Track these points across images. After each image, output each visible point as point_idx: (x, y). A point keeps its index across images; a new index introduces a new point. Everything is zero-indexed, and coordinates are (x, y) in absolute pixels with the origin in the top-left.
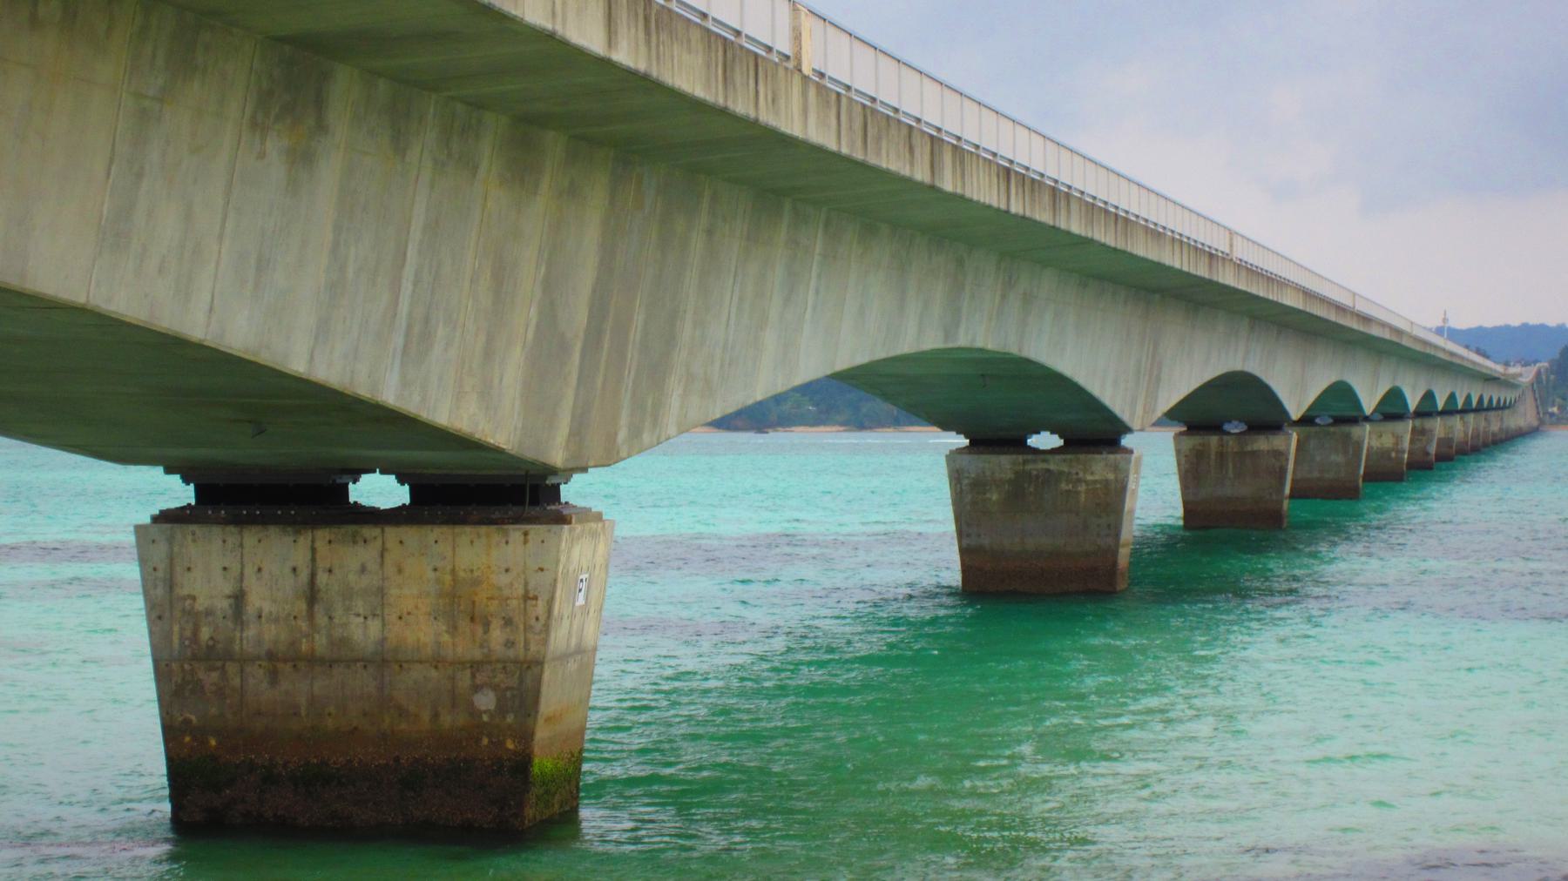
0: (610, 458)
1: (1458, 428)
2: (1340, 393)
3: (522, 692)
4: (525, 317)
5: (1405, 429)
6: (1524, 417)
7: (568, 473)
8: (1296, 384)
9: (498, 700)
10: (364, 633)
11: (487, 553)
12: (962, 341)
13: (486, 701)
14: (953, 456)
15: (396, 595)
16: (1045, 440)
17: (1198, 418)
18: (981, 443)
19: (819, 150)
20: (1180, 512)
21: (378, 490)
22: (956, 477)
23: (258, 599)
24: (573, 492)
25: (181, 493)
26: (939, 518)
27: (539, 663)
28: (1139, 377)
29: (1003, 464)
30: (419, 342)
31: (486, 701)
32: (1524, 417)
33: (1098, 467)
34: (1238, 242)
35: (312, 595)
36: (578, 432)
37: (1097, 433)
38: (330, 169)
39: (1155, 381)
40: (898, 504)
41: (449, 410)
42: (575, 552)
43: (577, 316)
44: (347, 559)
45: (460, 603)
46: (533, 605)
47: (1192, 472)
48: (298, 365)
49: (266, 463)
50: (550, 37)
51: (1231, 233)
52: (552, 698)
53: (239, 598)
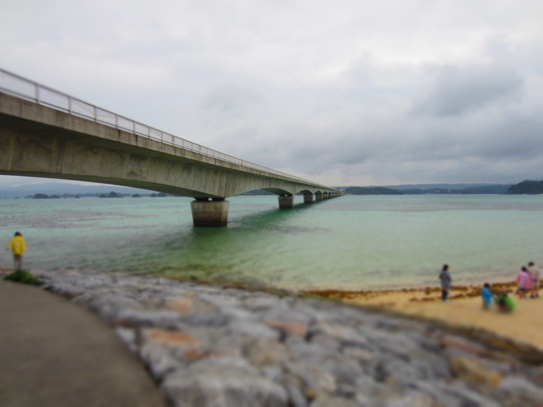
0: (229, 196)
1: (334, 195)
3: (220, 214)
5: (327, 195)
7: (225, 197)
8: (322, 191)
9: (305, 198)
10: (208, 210)
11: (218, 204)
12: (271, 187)
15: (210, 207)
16: (286, 196)
19: (245, 172)
21: (210, 199)
24: (226, 199)
25: (194, 199)
28: (313, 191)
29: (282, 197)
30: (205, 187)
32: (343, 193)
33: (290, 198)
34: (176, 139)
37: (311, 194)
38: (192, 174)
39: (295, 191)
42: (224, 204)
43: (224, 185)
44: (207, 205)
45: (216, 208)
46: (221, 208)
47: (316, 197)
49: (201, 198)
50: (207, 163)
51: (173, 136)
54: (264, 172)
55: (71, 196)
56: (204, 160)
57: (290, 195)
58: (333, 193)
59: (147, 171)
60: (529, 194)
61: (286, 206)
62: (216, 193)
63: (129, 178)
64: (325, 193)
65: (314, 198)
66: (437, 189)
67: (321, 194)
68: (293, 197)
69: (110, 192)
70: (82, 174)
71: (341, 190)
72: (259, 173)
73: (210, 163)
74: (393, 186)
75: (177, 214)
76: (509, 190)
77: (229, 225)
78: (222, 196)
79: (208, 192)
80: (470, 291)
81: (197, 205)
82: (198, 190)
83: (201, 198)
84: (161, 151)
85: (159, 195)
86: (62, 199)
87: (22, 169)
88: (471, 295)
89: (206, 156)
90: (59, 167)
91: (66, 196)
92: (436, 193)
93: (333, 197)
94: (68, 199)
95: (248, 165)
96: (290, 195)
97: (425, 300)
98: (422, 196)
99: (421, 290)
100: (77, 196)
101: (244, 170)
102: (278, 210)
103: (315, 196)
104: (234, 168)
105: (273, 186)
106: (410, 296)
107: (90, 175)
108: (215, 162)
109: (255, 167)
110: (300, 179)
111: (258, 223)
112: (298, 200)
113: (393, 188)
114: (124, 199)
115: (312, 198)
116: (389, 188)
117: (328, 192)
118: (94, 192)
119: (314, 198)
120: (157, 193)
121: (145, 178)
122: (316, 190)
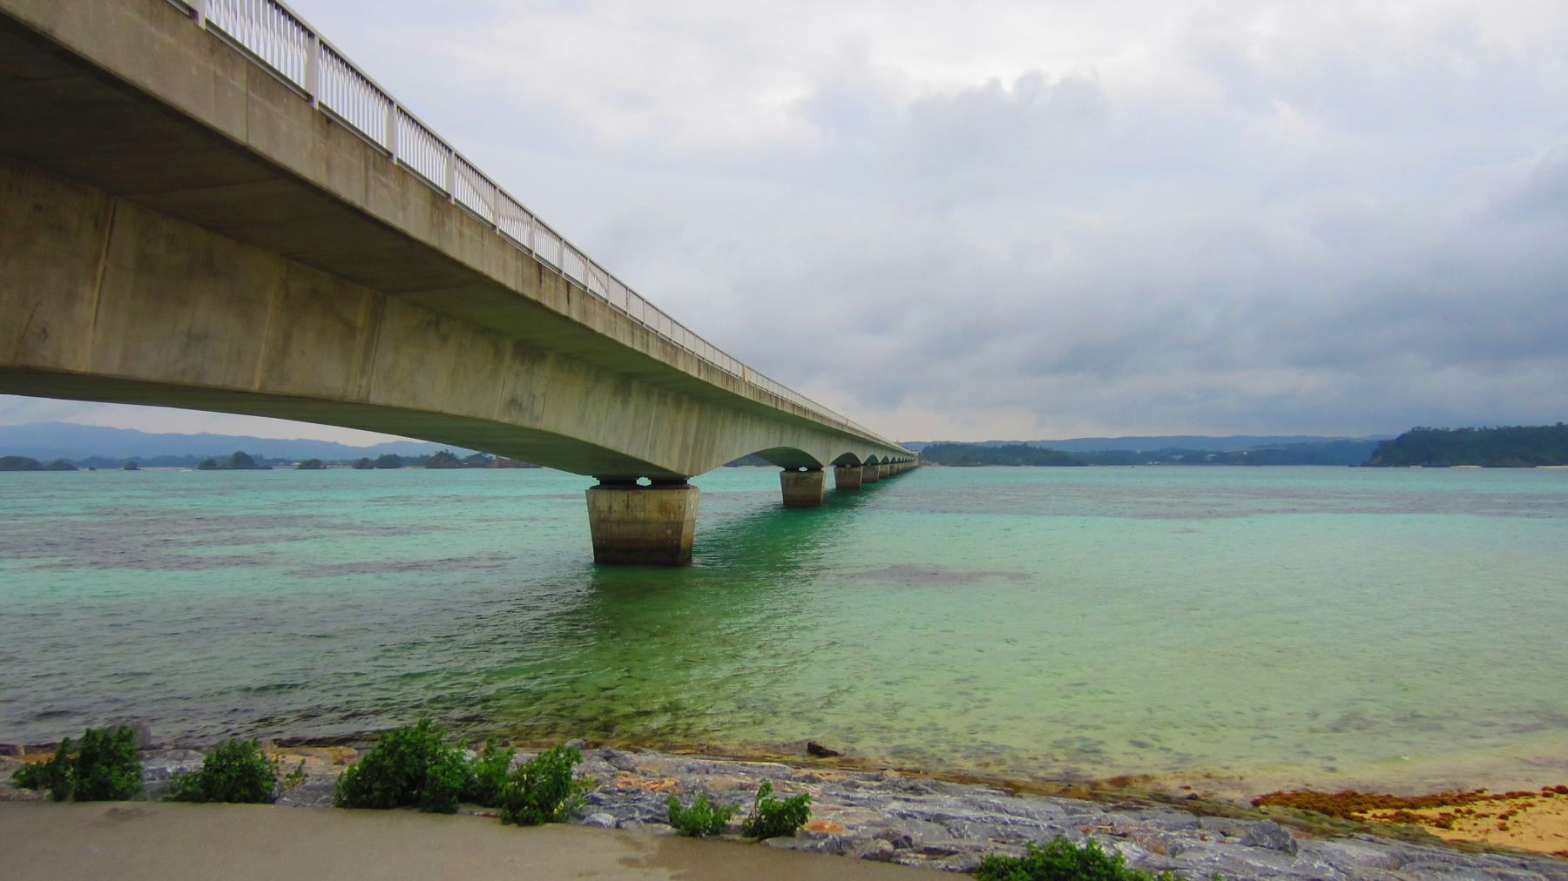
1: (901, 466)
3: (678, 527)
6: (916, 463)
8: (863, 456)
10: (640, 515)
11: (670, 496)
15: (648, 506)
16: (803, 469)
20: (780, 499)
28: (825, 454)
29: (793, 475)
33: (816, 475)
36: (691, 468)
37: (816, 467)
41: (660, 462)
42: (691, 496)
43: (691, 440)
44: (637, 499)
45: (663, 508)
46: (681, 508)
47: (838, 477)
49: (616, 474)
52: (685, 531)
55: (110, 464)
59: (544, 395)
61: (802, 500)
62: (672, 464)
63: (506, 420)
65: (829, 481)
66: (1176, 452)
67: (856, 463)
68: (829, 476)
69: (230, 453)
70: (411, 405)
75: (542, 522)
76: (1375, 455)
77: (696, 560)
81: (604, 499)
83: (616, 474)
84: (609, 335)
85: (471, 463)
86: (84, 473)
87: (288, 389)
90: (364, 383)
91: (95, 463)
92: (1173, 462)
94: (101, 474)
98: (1138, 469)
100: (132, 466)
102: (776, 506)
103: (866, 472)
107: (426, 407)
114: (278, 473)
115: (819, 483)
118: (182, 454)
119: (829, 481)
120: (462, 453)
121: (537, 419)
122: (838, 451)
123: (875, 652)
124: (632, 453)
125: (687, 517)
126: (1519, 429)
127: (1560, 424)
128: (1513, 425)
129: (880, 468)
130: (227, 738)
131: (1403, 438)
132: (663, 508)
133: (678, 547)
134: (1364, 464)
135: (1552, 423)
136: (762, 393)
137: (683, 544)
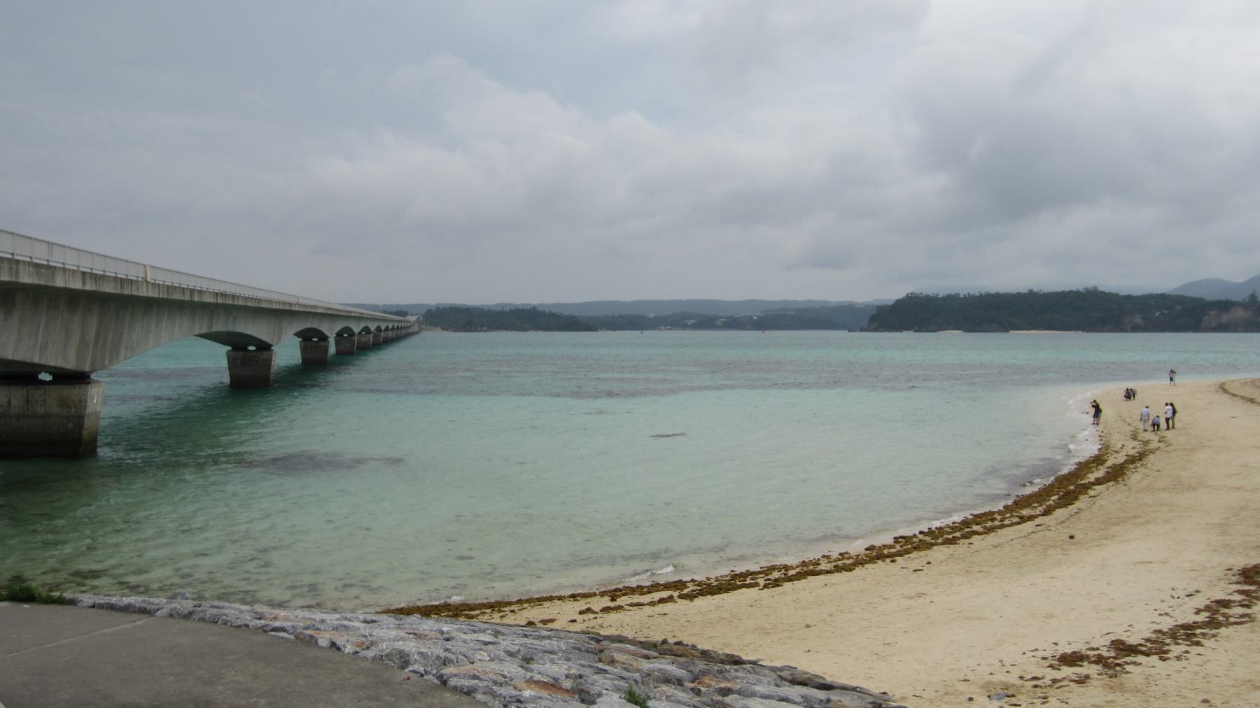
1: (390, 334)
2: (347, 330)
3: (80, 419)
4: (76, 339)
6: (416, 328)
7: (92, 372)
8: (356, 328)
11: (73, 392)
13: (70, 425)
14: (228, 352)
16: (252, 348)
17: (339, 335)
18: (304, 340)
20: (300, 361)
22: (229, 357)
23: (14, 402)
24: (93, 376)
26: (224, 363)
27: (83, 417)
31: (70, 425)
33: (265, 355)
35: (28, 401)
36: (93, 363)
37: (324, 338)
40: (213, 363)
41: (52, 363)
43: (91, 336)
44: (37, 394)
45: (64, 403)
46: (82, 404)
48: (10, 357)
52: (88, 423)
53: (9, 403)
54: (200, 292)
56: (59, 282)
57: (265, 347)
58: (387, 329)
60: (919, 331)
61: (252, 379)
64: (367, 330)
67: (352, 334)
71: (412, 319)
72: (187, 298)
73: (72, 286)
74: (565, 305)
76: (872, 319)
77: (104, 452)
78: (87, 368)
79: (36, 360)
80: (691, 587)
82: (28, 360)
88: (690, 597)
89: (64, 270)
92: (685, 327)
93: (388, 342)
95: (160, 278)
96: (265, 347)
97: (606, 610)
99: (602, 594)
101: (151, 294)
102: (219, 388)
104: (127, 292)
105: (220, 326)
106: (582, 604)
108: (84, 283)
109: (177, 281)
110: (294, 300)
111: (181, 439)
112: (287, 353)
113: (566, 313)
115: (326, 348)
116: (556, 311)
117: (373, 327)
123: (354, 518)
124: (19, 357)
125: (89, 410)
126: (997, 295)
127: (1031, 292)
128: (993, 291)
129: (382, 334)
130: (1127, 482)
131: (899, 303)
132: (64, 403)
133: (80, 440)
134: (862, 330)
135: (1025, 290)
136: (170, 288)
137: (85, 434)
